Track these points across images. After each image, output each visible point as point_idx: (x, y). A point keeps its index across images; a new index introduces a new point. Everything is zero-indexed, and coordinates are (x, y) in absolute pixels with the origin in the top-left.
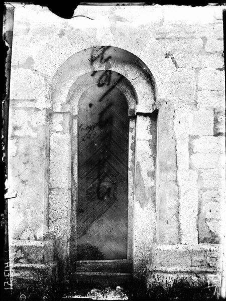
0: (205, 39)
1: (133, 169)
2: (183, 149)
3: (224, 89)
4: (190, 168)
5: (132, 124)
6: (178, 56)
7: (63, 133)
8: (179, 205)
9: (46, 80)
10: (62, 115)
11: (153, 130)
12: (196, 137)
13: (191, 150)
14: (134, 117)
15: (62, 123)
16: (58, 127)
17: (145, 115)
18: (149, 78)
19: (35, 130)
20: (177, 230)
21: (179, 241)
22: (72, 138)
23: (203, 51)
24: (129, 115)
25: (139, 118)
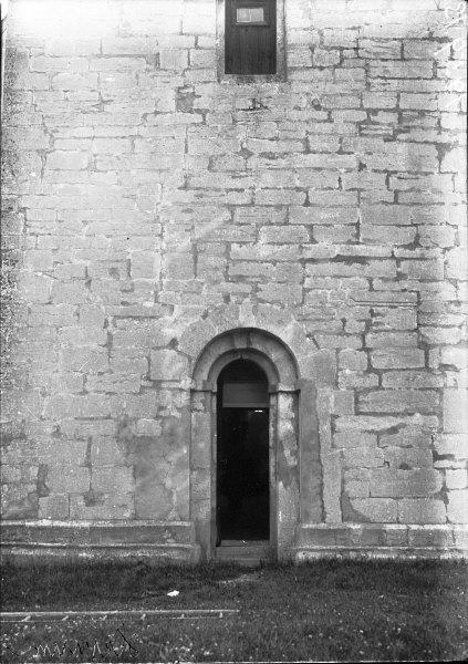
0: (344, 321)
1: (274, 448)
2: (326, 428)
3: (465, 168)
4: (50, 303)
5: (273, 401)
6: (320, 338)
7: (205, 411)
8: (322, 484)
9: (190, 361)
10: (202, 394)
11: (295, 406)
12: (336, 417)
13: (333, 430)
14: (276, 393)
15: (204, 402)
16: (201, 406)
17: (287, 393)
18: (291, 358)
19: (179, 409)
20: (320, 510)
21: (323, 520)
22: (212, 416)
23: (342, 333)
24: (270, 391)
25: (281, 397)
